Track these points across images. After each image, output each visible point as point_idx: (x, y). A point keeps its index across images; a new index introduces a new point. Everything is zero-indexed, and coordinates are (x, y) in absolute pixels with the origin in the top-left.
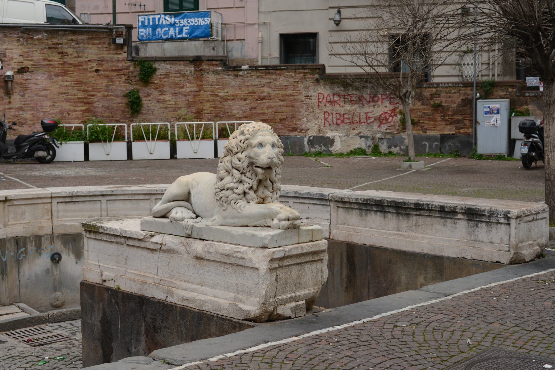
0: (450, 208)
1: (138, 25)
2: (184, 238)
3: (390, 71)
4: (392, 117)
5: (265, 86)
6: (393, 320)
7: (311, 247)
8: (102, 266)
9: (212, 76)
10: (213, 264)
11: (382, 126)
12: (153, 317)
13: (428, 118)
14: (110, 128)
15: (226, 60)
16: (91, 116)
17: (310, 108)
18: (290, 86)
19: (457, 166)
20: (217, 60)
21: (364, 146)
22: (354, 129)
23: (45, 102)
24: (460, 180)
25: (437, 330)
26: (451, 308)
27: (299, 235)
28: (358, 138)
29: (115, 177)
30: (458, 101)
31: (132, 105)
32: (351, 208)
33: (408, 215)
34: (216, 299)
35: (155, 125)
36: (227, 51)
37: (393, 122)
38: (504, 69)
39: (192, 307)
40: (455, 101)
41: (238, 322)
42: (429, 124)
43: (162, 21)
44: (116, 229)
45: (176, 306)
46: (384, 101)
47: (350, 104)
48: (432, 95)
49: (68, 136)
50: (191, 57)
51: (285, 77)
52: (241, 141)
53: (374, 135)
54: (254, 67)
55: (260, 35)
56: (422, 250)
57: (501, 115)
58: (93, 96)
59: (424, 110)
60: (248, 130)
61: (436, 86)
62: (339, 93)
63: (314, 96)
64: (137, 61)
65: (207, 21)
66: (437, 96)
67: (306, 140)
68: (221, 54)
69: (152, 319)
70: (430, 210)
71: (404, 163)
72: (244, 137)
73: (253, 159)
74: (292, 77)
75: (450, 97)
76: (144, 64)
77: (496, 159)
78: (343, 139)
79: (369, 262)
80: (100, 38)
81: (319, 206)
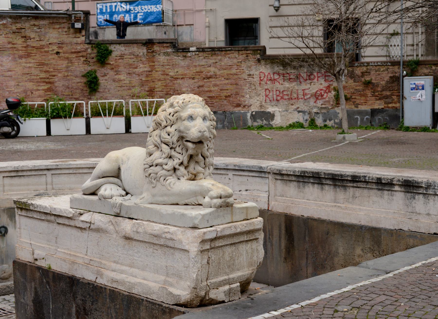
0: (387, 180)
1: (97, 12)
2: (113, 217)
3: (325, 52)
4: (327, 93)
5: (212, 66)
6: (334, 303)
7: (245, 226)
8: (34, 244)
9: (163, 58)
10: (142, 244)
11: (318, 101)
12: (84, 298)
13: (360, 94)
14: (70, 106)
15: (176, 43)
16: (53, 95)
17: (252, 86)
18: (234, 65)
19: (387, 138)
20: (167, 43)
21: (301, 120)
22: (292, 105)
23: (10, 82)
24: (390, 150)
25: (380, 316)
26: (394, 288)
27: (232, 214)
28: (296, 112)
29: (72, 151)
30: (387, 78)
31: (90, 85)
32: (289, 180)
33: (345, 187)
34: (145, 282)
35: (111, 103)
36: (177, 35)
37: (328, 98)
38: (427, 50)
39: (121, 289)
40: (384, 78)
41: (168, 307)
42: (360, 99)
43: (119, 9)
44: (46, 207)
45: (105, 288)
46: (319, 79)
47: (289, 82)
48: (363, 73)
49: (32, 113)
50: (144, 40)
51: (229, 57)
52: (170, 114)
53: (311, 110)
54: (201, 48)
55: (207, 21)
56: (360, 222)
57: (426, 91)
58: (54, 76)
59: (356, 87)
60: (178, 102)
61: (367, 65)
62: (278, 72)
63: (256, 75)
64: (94, 44)
65: (159, 7)
66: (368, 74)
67: (249, 115)
68: (172, 37)
69: (83, 300)
70: (367, 182)
71: (339, 135)
72: (173, 109)
73: (182, 132)
74: (236, 58)
75: (379, 74)
76: (101, 46)
77: (422, 131)
78: (283, 114)
79: (307, 233)
80: (60, 23)
81: (257, 178)
